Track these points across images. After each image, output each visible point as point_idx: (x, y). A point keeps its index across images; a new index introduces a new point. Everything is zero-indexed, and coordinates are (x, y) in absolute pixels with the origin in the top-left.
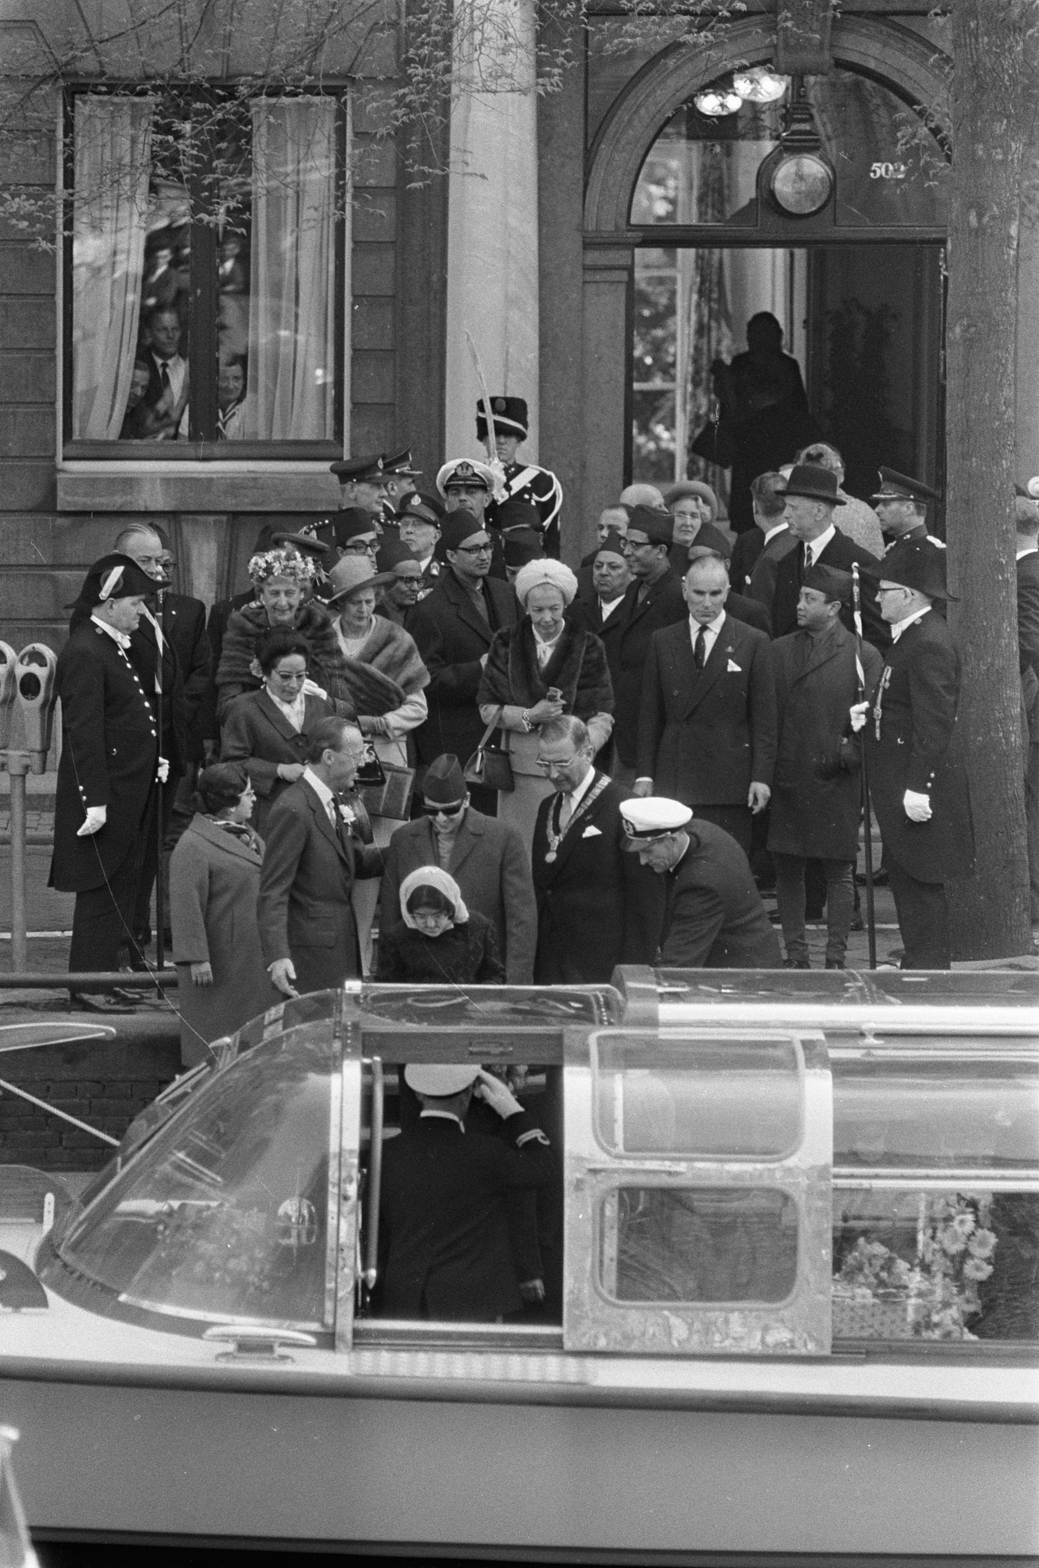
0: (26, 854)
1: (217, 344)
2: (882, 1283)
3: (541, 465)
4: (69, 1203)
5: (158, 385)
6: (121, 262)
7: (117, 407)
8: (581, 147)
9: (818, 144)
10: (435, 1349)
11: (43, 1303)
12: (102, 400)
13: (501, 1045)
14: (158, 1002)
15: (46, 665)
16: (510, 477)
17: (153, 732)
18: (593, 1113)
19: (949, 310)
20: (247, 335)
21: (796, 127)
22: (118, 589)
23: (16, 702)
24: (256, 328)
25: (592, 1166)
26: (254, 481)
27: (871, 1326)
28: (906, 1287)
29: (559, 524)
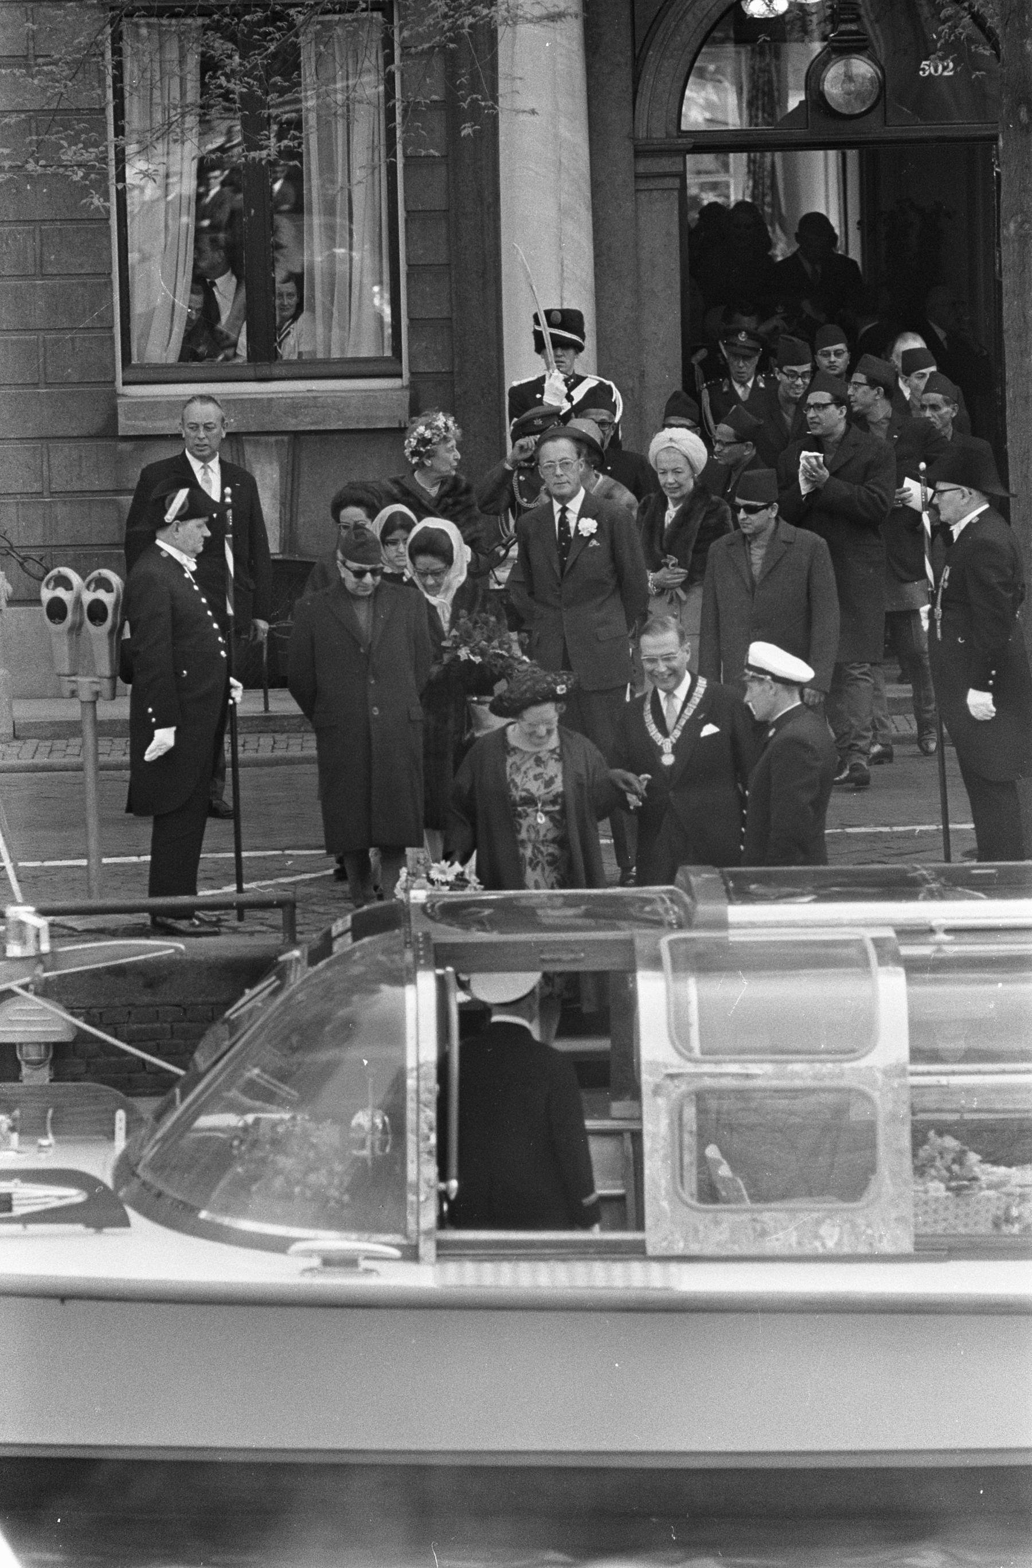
0: (98, 781)
1: (273, 264)
2: (953, 1177)
3: (599, 375)
4: (141, 1120)
5: (209, 310)
6: (174, 184)
7: (176, 329)
8: (629, 54)
9: (866, 43)
10: (519, 1258)
11: (125, 1222)
12: (159, 324)
13: (572, 951)
14: (236, 923)
15: (112, 591)
16: (570, 388)
17: (223, 653)
18: (669, 1018)
19: (1003, 205)
20: (303, 255)
21: (843, 27)
22: (184, 511)
23: (83, 629)
24: (311, 249)
25: (671, 1071)
26: (313, 401)
27: (945, 1220)
28: (975, 1179)
29: (620, 433)
